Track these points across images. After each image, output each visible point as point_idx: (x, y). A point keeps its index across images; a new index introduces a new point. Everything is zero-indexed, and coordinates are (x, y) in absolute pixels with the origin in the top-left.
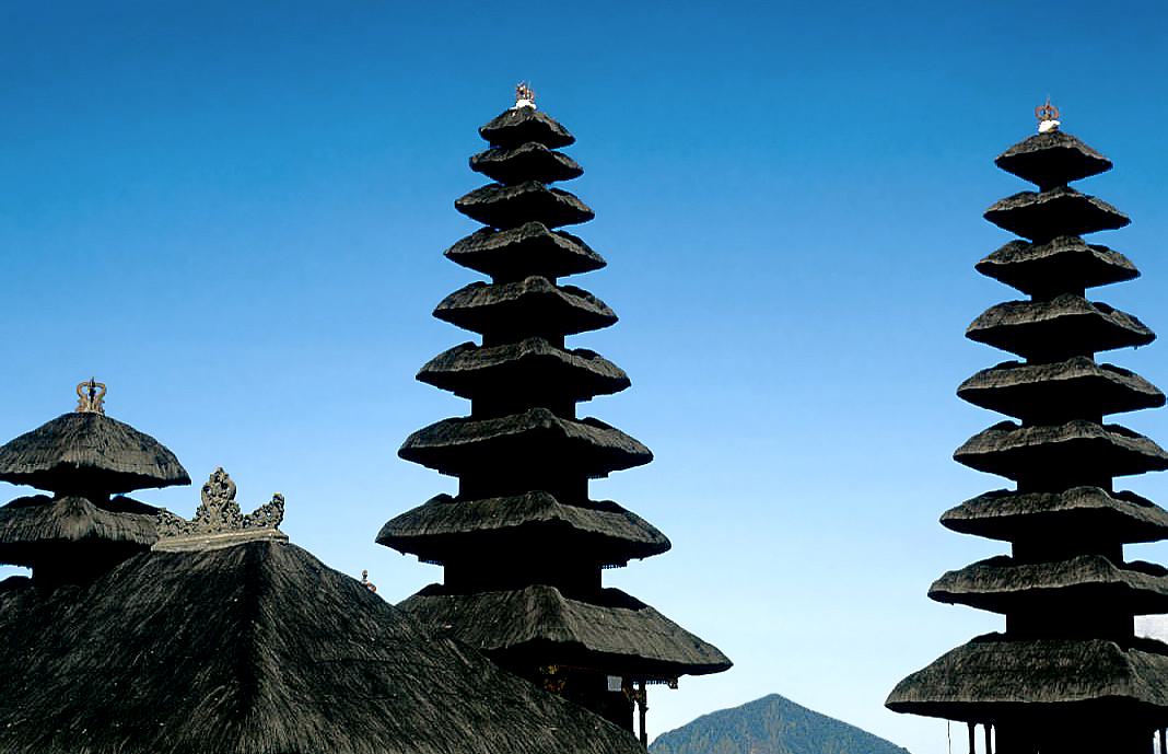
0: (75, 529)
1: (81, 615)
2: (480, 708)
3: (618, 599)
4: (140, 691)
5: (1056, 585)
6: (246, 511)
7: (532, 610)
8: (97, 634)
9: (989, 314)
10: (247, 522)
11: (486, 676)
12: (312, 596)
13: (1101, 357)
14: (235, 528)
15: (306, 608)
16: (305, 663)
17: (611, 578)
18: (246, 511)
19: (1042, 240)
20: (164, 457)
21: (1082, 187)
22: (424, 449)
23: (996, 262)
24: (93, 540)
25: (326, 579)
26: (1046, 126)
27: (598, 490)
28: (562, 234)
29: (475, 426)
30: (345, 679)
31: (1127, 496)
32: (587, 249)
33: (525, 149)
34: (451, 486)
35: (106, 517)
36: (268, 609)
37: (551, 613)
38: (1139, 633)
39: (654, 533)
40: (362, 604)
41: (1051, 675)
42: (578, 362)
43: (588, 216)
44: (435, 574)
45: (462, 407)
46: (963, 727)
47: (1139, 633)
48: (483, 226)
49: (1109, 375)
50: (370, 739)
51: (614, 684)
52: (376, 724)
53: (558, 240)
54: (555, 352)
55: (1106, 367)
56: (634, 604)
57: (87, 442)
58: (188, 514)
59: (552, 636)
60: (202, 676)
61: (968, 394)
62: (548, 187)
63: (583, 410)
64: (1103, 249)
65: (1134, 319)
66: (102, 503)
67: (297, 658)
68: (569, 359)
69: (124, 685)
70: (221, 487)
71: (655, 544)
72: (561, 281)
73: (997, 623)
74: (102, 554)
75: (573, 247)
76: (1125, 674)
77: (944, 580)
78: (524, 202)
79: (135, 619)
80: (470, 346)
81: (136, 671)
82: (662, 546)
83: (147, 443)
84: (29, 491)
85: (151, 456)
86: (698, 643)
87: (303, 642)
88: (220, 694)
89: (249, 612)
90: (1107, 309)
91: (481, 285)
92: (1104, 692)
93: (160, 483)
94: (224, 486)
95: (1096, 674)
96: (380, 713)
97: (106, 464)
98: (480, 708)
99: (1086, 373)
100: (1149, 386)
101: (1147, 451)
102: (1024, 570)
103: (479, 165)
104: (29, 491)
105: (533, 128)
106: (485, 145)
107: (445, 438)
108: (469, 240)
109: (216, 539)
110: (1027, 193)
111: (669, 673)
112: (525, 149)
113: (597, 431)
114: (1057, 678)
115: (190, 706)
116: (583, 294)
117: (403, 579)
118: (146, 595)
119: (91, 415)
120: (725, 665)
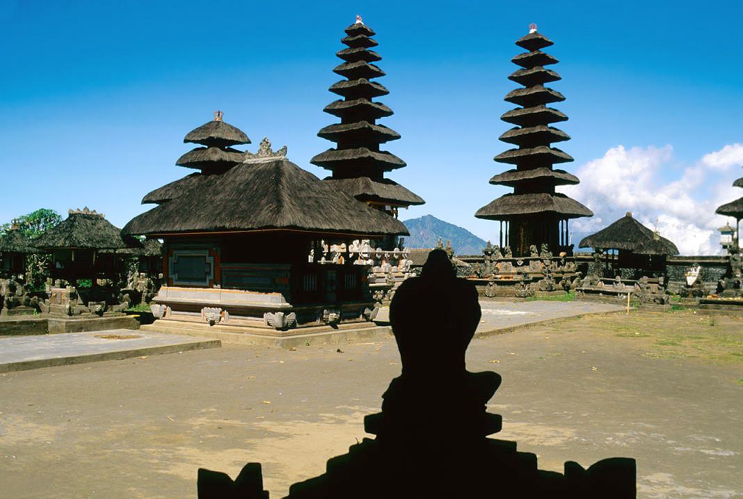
0: (215, 158)
1: (222, 183)
2: (353, 213)
3: (388, 182)
4: (243, 205)
5: (531, 177)
6: (275, 151)
7: (361, 186)
8: (227, 189)
9: (512, 93)
10: (275, 154)
11: (353, 203)
12: (297, 178)
13: (548, 105)
14: (271, 156)
15: (295, 181)
16: (297, 198)
17: (386, 175)
18: (275, 151)
19: (530, 68)
20: (243, 135)
21: (543, 50)
22: (325, 134)
23: (515, 76)
24: (221, 162)
25: (301, 173)
26: (532, 31)
27: (382, 147)
28: (371, 65)
29: (342, 126)
30: (310, 202)
31: (554, 149)
32: (380, 70)
33: (359, 36)
34: (334, 145)
35: (224, 153)
36: (283, 181)
37: (367, 186)
38: (557, 191)
39: (401, 161)
40: (313, 180)
41: (528, 205)
42: (377, 106)
43: (380, 59)
44: (330, 173)
45: (338, 120)
46: (499, 222)
47: (557, 191)
48: (345, 61)
49: (551, 111)
50: (318, 221)
51: (388, 208)
52: (319, 216)
53: (371, 67)
54: (369, 103)
55: (550, 108)
56: (394, 183)
57: (218, 130)
58: (255, 152)
59: (368, 193)
60: (264, 202)
61: (504, 119)
62: (367, 49)
63: (378, 122)
64: (550, 71)
65: (559, 93)
66: (223, 150)
67: (294, 196)
68: (373, 105)
69: (238, 205)
70: (265, 142)
71: (401, 165)
72: (371, 80)
73: (511, 190)
74: (223, 167)
75: (375, 69)
76: (552, 203)
77: (494, 178)
78: (359, 52)
79: (240, 184)
80: (341, 101)
81: (241, 200)
82: (405, 165)
83: (237, 131)
84: (199, 146)
85: (238, 135)
86: (415, 196)
87: (295, 192)
88: (270, 207)
89: (278, 182)
90: (551, 90)
91: (344, 81)
92: (546, 209)
93: (241, 143)
94: (267, 143)
95: (543, 204)
96: (320, 213)
97: (224, 137)
98: (353, 213)
99: (544, 110)
100: (563, 114)
101: (562, 135)
102: (521, 173)
103: (344, 42)
104: (199, 146)
105: (361, 30)
106: (346, 35)
107: (333, 130)
108: (340, 66)
109: (264, 159)
110: (525, 53)
111: (405, 204)
112: (359, 36)
113: (383, 129)
114: (530, 205)
115: (261, 210)
116: (378, 84)
117: (323, 173)
118: (241, 177)
119: (219, 122)
120: (423, 203)
